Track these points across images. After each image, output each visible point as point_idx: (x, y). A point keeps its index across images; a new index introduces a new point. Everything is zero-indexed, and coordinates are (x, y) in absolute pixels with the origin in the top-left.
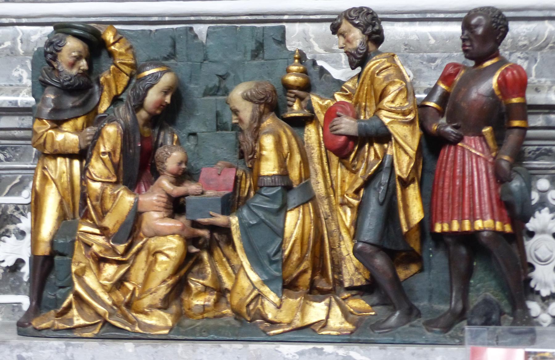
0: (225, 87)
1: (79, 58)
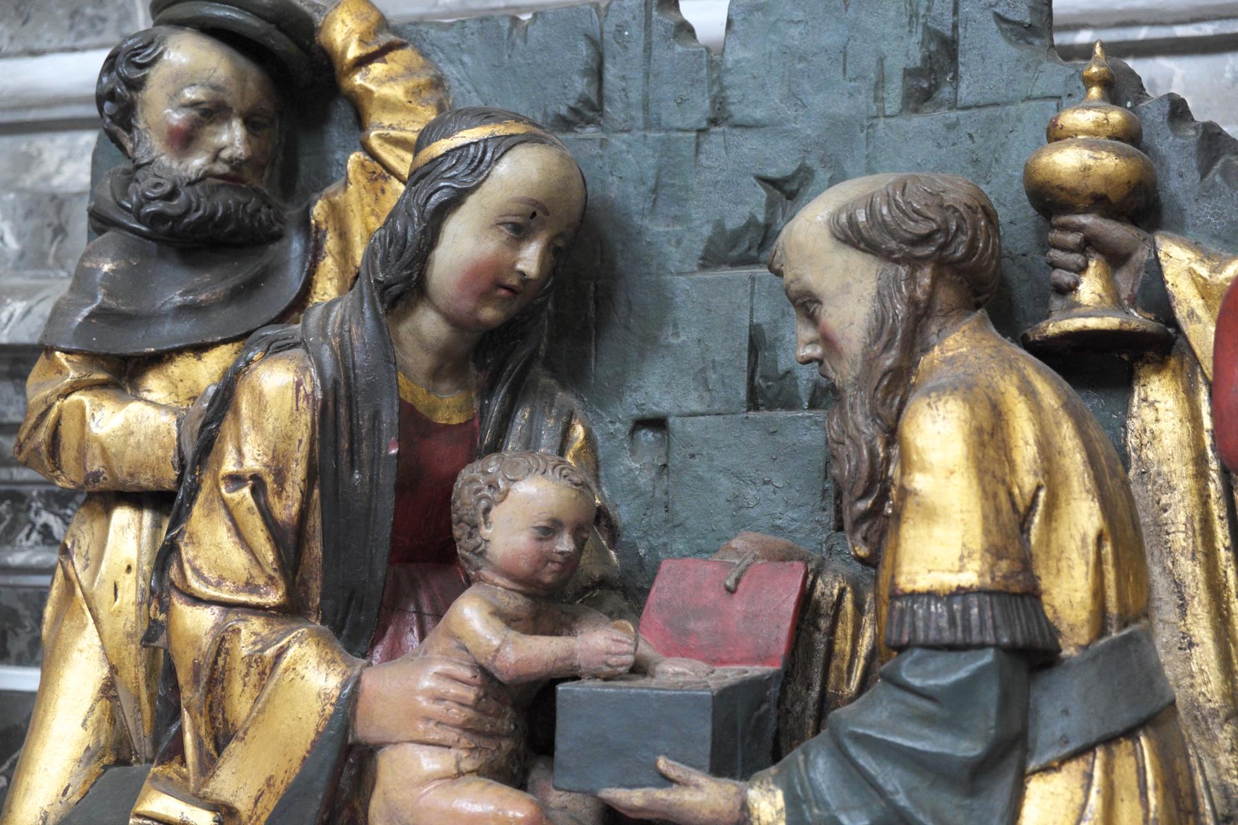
1: (212, 112)
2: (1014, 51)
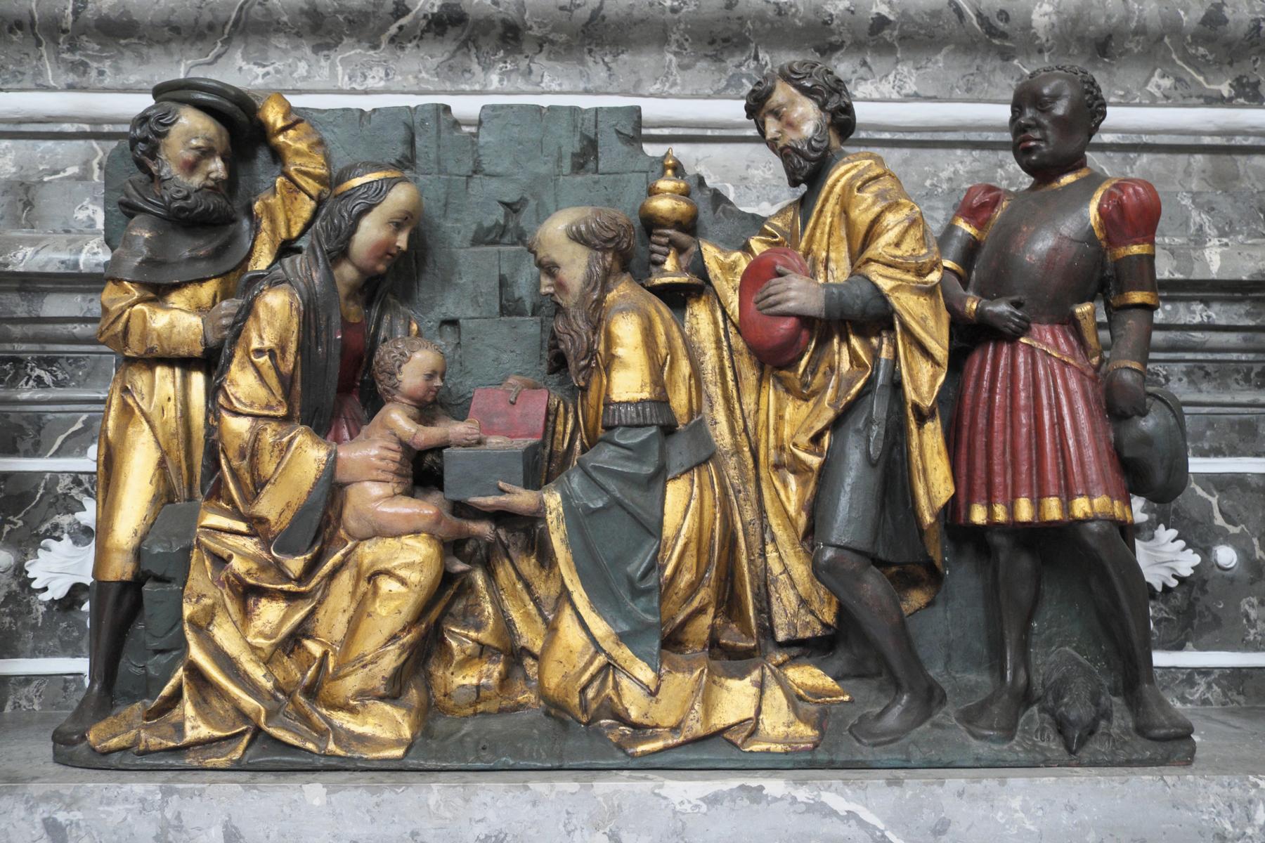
1: (206, 153)
2: (626, 148)
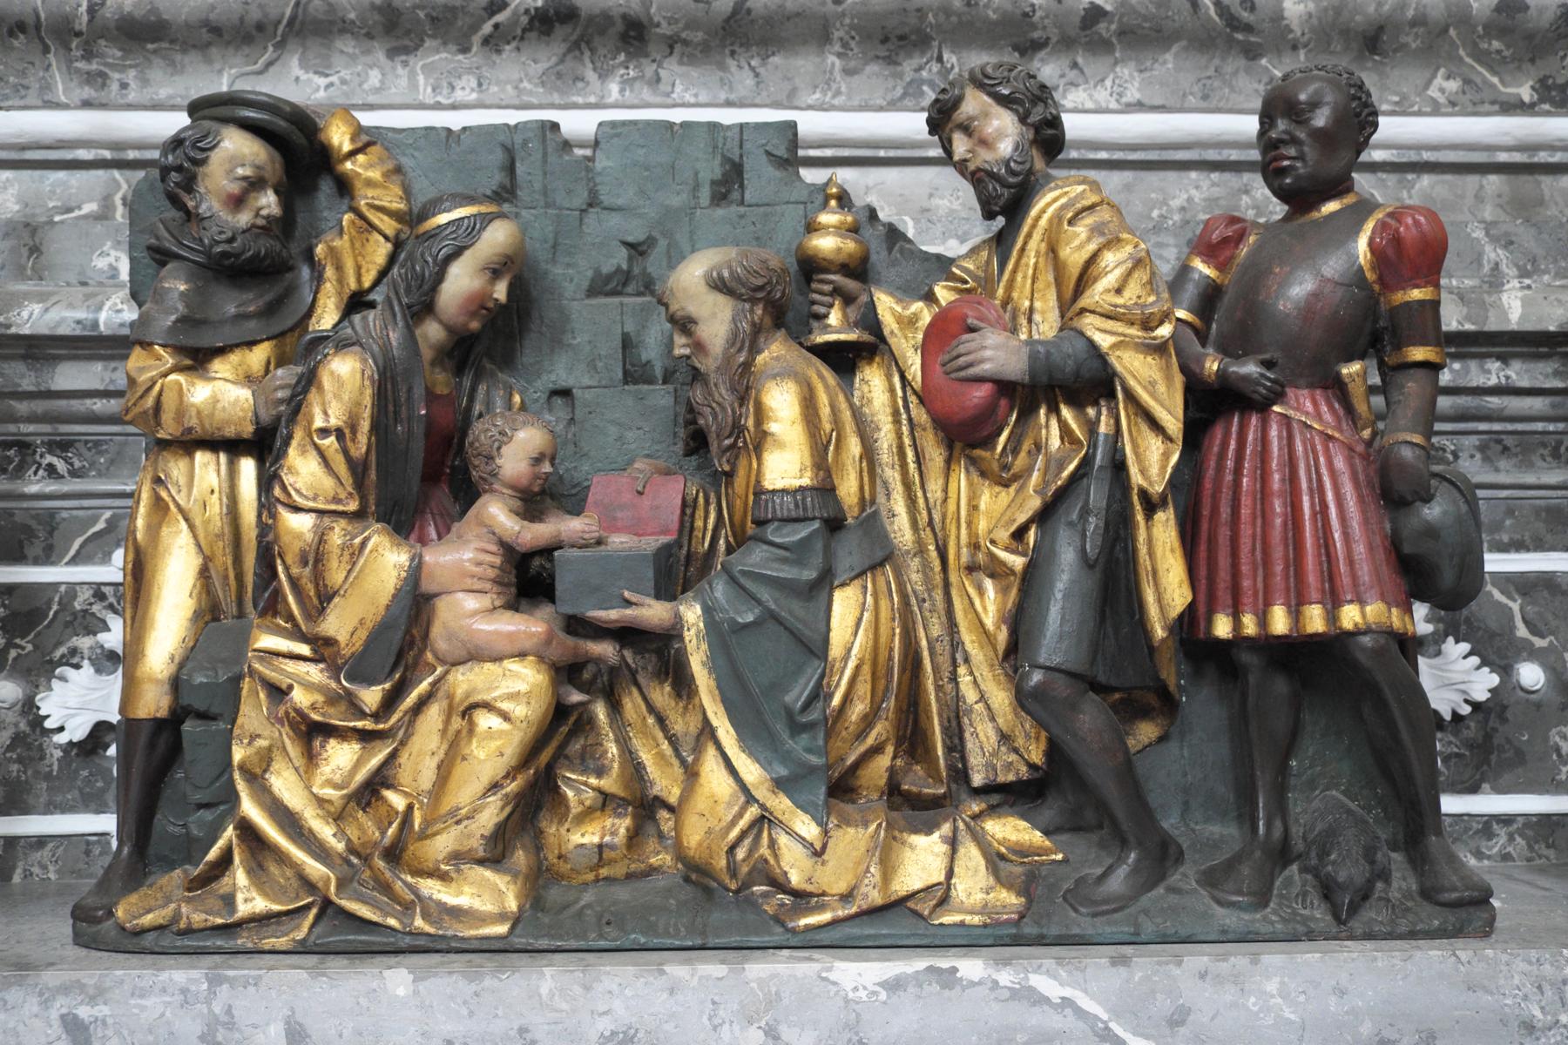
0: (644, 272)
1: (255, 184)
2: (778, 174)
